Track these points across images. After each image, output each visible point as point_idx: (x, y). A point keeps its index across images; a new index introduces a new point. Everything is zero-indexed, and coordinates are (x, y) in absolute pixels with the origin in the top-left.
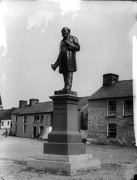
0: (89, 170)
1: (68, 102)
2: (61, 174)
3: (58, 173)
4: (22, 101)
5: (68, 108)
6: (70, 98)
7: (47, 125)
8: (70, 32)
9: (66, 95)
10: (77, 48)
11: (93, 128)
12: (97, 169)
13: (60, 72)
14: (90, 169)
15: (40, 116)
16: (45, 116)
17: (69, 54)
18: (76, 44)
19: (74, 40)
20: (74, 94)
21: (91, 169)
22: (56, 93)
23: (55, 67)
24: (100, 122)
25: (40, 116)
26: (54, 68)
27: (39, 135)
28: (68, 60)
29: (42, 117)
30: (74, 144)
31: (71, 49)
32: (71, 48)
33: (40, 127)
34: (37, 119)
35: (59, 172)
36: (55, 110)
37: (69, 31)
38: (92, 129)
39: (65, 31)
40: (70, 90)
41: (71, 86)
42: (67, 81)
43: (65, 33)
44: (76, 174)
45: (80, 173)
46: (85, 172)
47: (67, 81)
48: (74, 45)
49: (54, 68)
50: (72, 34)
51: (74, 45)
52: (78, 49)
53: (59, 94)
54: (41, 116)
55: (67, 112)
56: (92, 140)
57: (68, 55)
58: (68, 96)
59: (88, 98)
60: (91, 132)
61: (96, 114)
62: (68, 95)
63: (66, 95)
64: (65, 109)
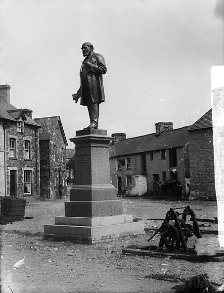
0: (124, 237)
1: (92, 145)
2: (81, 242)
3: (78, 241)
4: (162, 123)
5: (92, 152)
6: (94, 139)
7: (136, 174)
8: (93, 48)
9: (89, 135)
10: (101, 69)
11: (198, 174)
12: (137, 235)
13: (83, 103)
14: (125, 235)
15: (126, 160)
16: (132, 159)
17: (91, 79)
18: (100, 64)
19: (97, 59)
20: (102, 132)
21: (128, 235)
22: (78, 133)
23: (77, 97)
24: (208, 164)
25: (126, 160)
26: (75, 98)
27: (125, 191)
28: (90, 87)
29: (129, 162)
30: (101, 201)
31: (94, 73)
32: (93, 71)
33: (127, 176)
34: (122, 165)
35: (79, 240)
36: (78, 156)
37: (92, 47)
38: (197, 176)
39: (85, 48)
40: (96, 128)
41: (97, 123)
42: (93, 114)
43: (87, 50)
44: (100, 241)
45: (107, 241)
46: (117, 239)
47: (93, 114)
48: (97, 66)
49: (75, 98)
50: (95, 51)
51: (97, 66)
52: (105, 72)
53: (81, 135)
54: (127, 159)
55: (91, 159)
56: (198, 193)
57: (90, 80)
58: (90, 137)
59: (189, 129)
60: (196, 182)
61: (201, 152)
62: (91, 135)
63: (89, 135)
64: (89, 155)
